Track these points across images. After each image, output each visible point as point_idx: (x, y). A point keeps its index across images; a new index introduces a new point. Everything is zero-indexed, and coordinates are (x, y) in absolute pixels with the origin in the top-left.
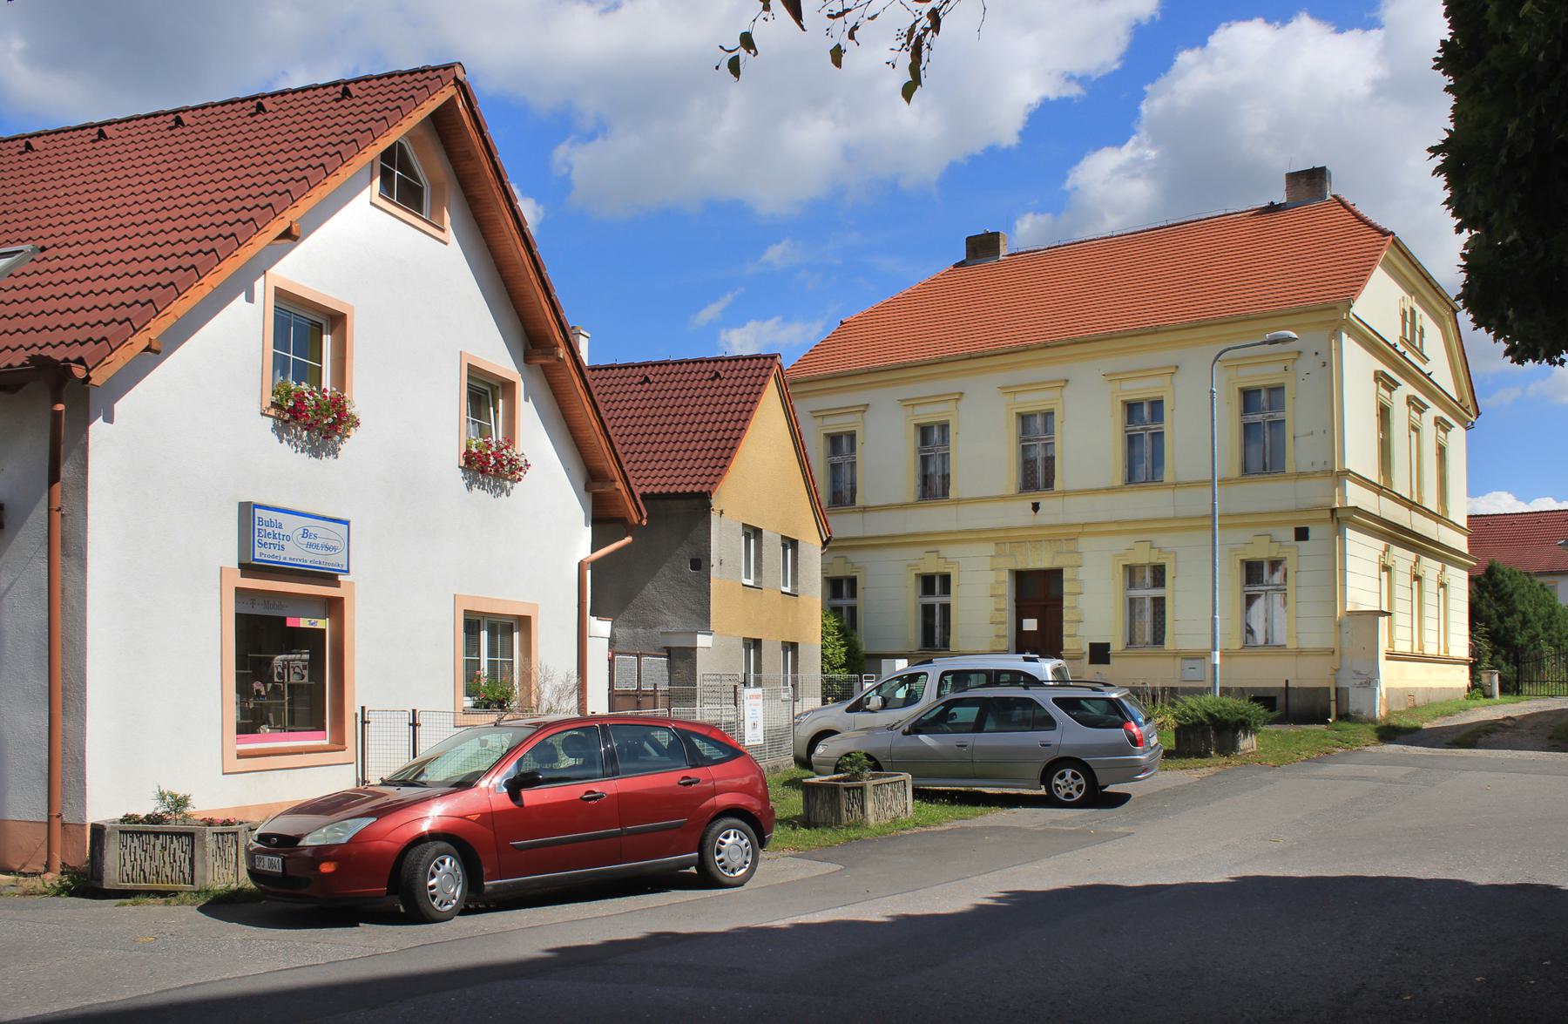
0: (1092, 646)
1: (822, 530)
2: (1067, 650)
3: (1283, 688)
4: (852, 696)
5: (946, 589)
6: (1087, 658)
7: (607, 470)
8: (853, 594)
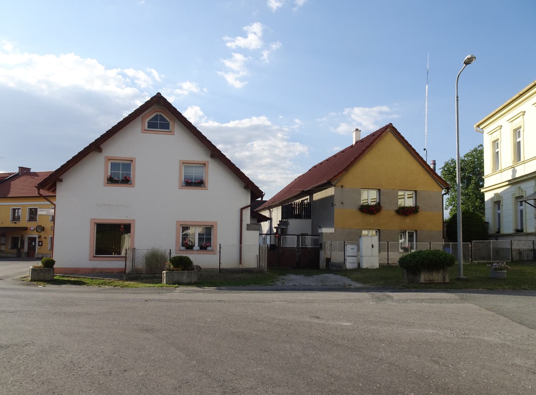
1: (437, 181)
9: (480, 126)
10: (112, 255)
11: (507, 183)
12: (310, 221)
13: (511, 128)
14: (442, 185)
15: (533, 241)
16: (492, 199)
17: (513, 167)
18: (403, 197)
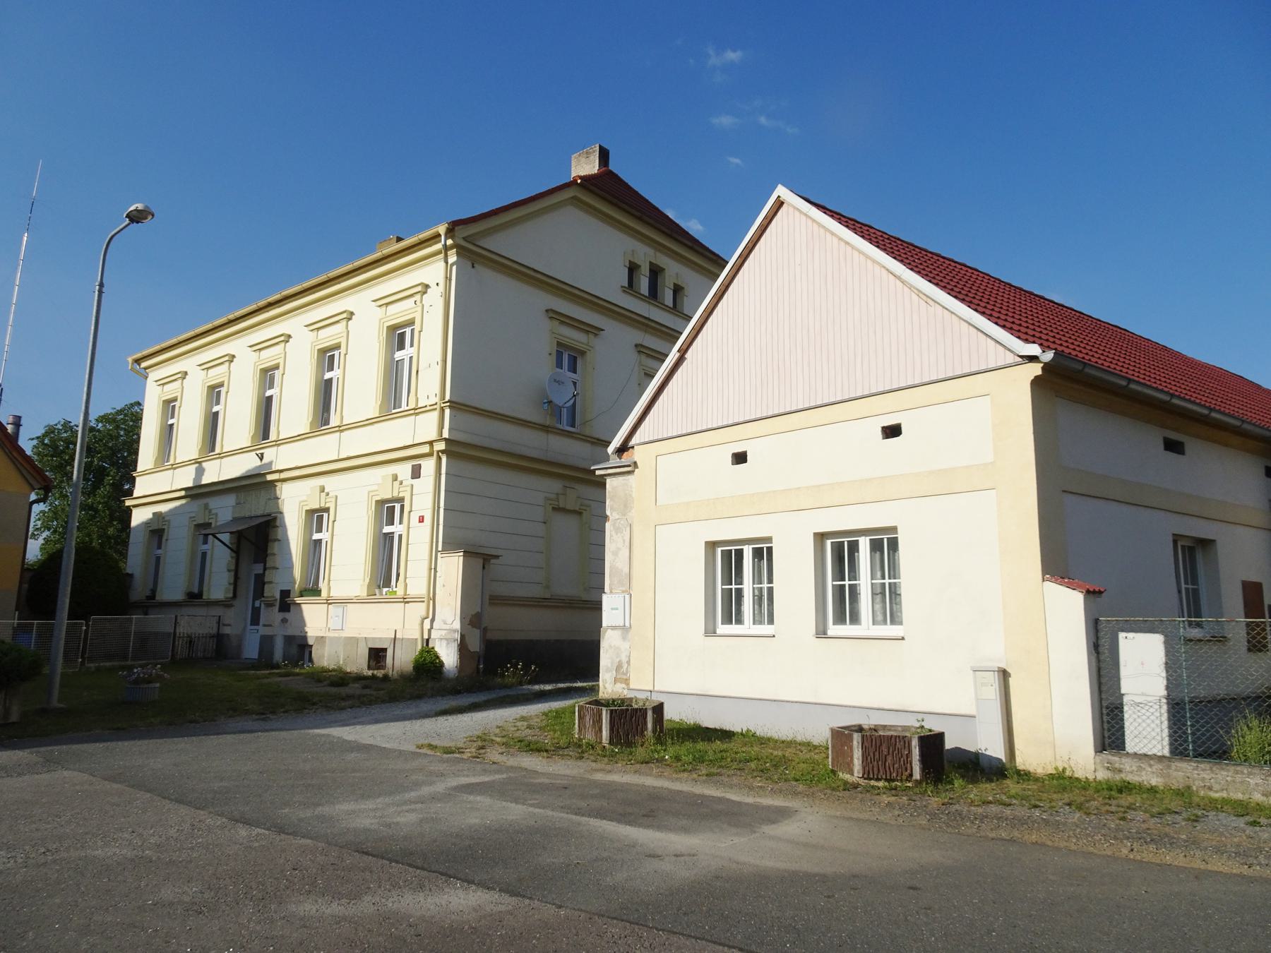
11: (183, 493)
17: (198, 462)
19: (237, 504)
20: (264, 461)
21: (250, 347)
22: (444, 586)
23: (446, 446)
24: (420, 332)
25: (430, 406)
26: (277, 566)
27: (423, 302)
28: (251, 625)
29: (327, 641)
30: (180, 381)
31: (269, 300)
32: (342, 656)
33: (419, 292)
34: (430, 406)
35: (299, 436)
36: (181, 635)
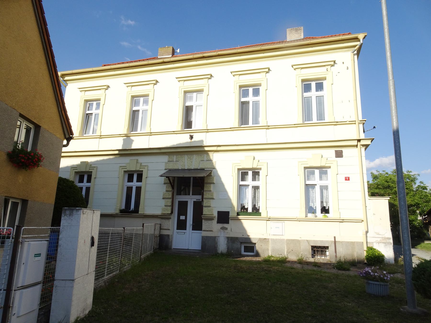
0: (219, 213)
1: (63, 122)
2: (204, 215)
3: (332, 242)
4: (366, 159)
5: (140, 179)
6: (216, 220)
7: (146, 255)
8: (89, 181)
9: (65, 76)
10: (410, 229)
11: (117, 152)
12: (241, 101)
13: (181, 88)
14: (67, 131)
15: (159, 225)
16: (72, 168)
17: (127, 136)
18: (354, 122)
19: (169, 161)
20: (193, 140)
21: (177, 78)
22: (374, 214)
23: (61, 154)
24: (103, 105)
25: (349, 122)
26: (214, 198)
27: (106, 93)
28: (177, 229)
29: (270, 241)
30: (104, 90)
31: (94, 69)
32: (286, 250)
33: (208, 78)
34: (349, 122)
35: (231, 128)
36: (155, 236)
